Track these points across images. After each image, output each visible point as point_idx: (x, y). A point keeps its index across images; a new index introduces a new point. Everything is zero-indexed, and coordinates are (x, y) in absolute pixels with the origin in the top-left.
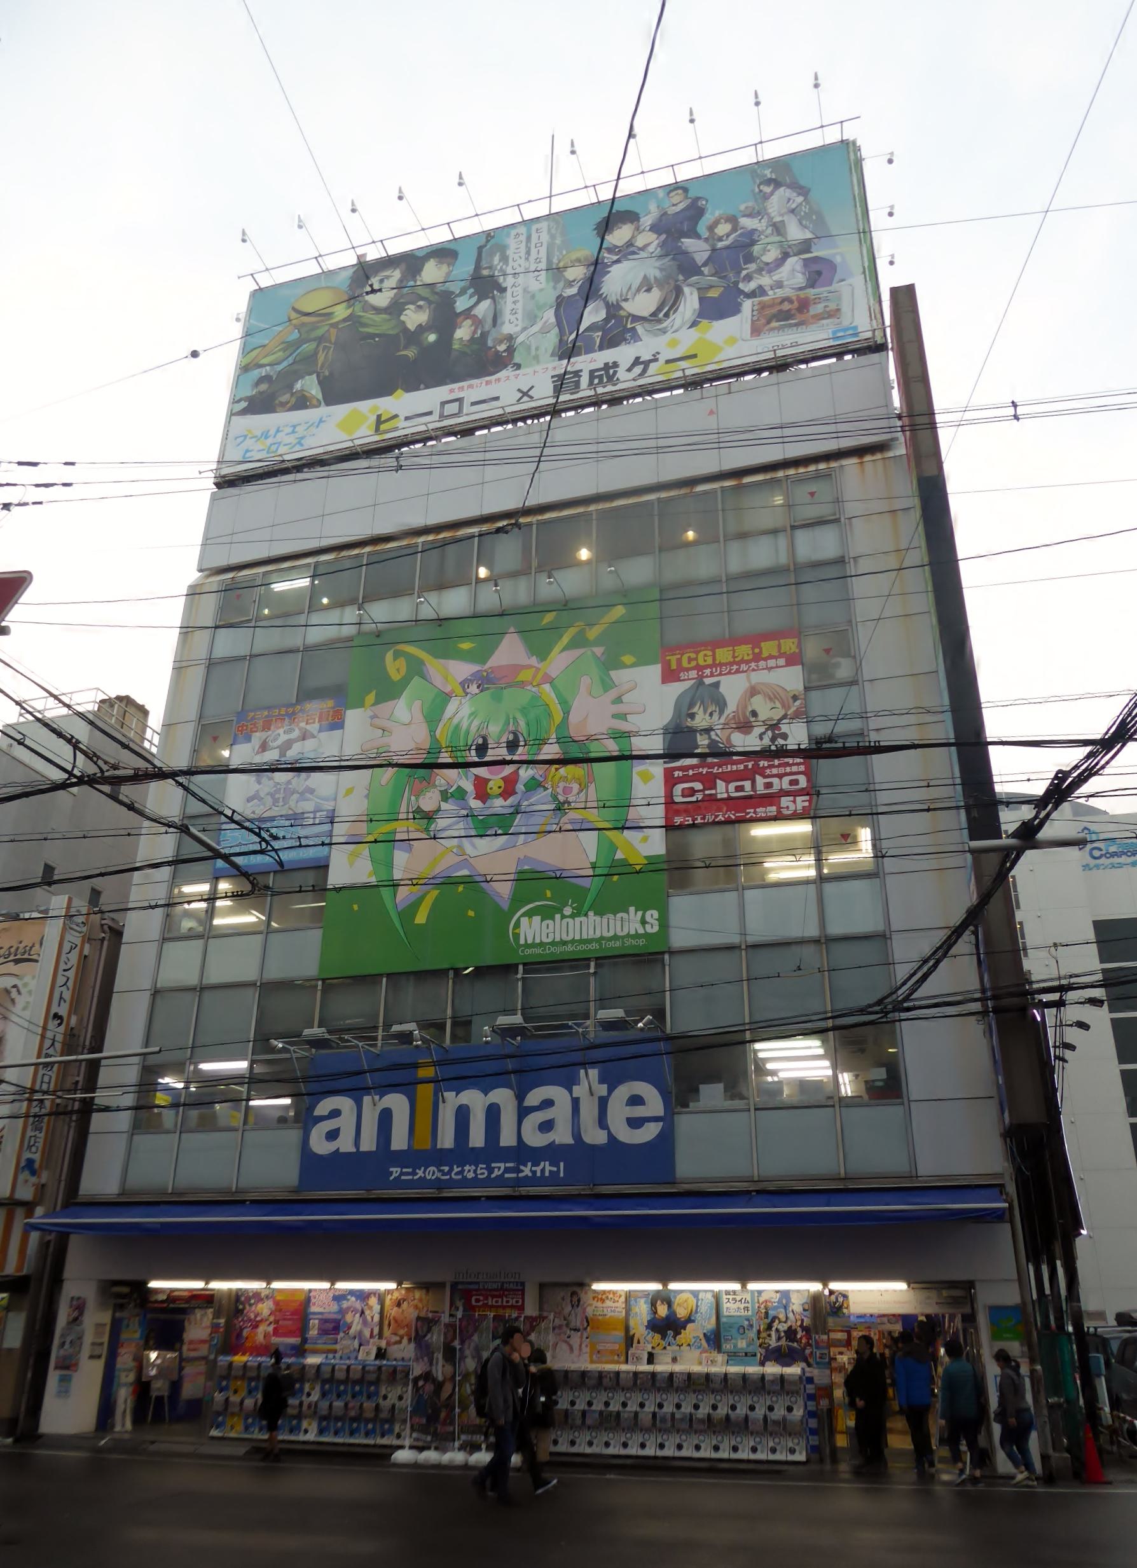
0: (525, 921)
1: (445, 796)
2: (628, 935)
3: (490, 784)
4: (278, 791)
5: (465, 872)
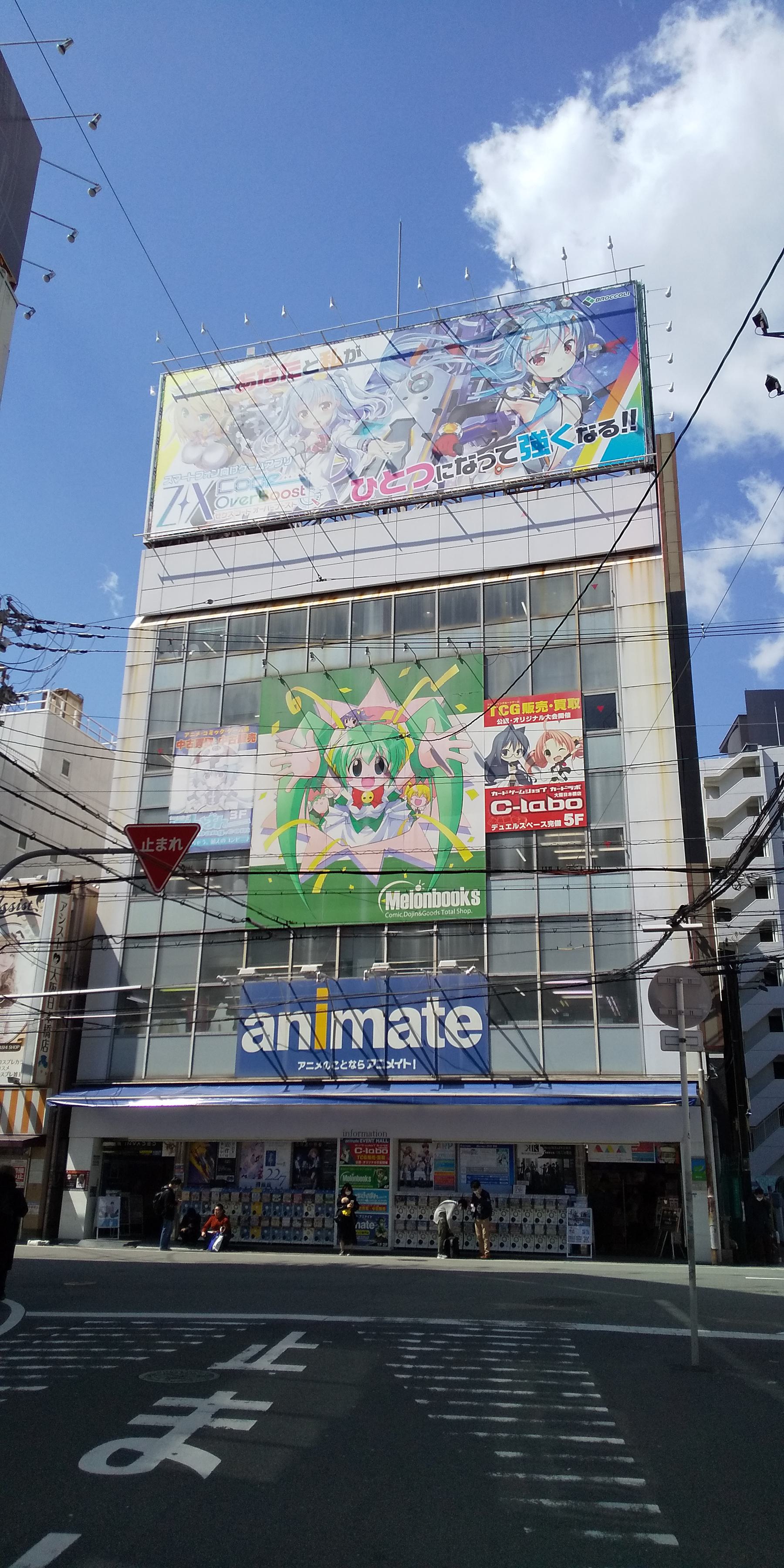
1: (332, 802)
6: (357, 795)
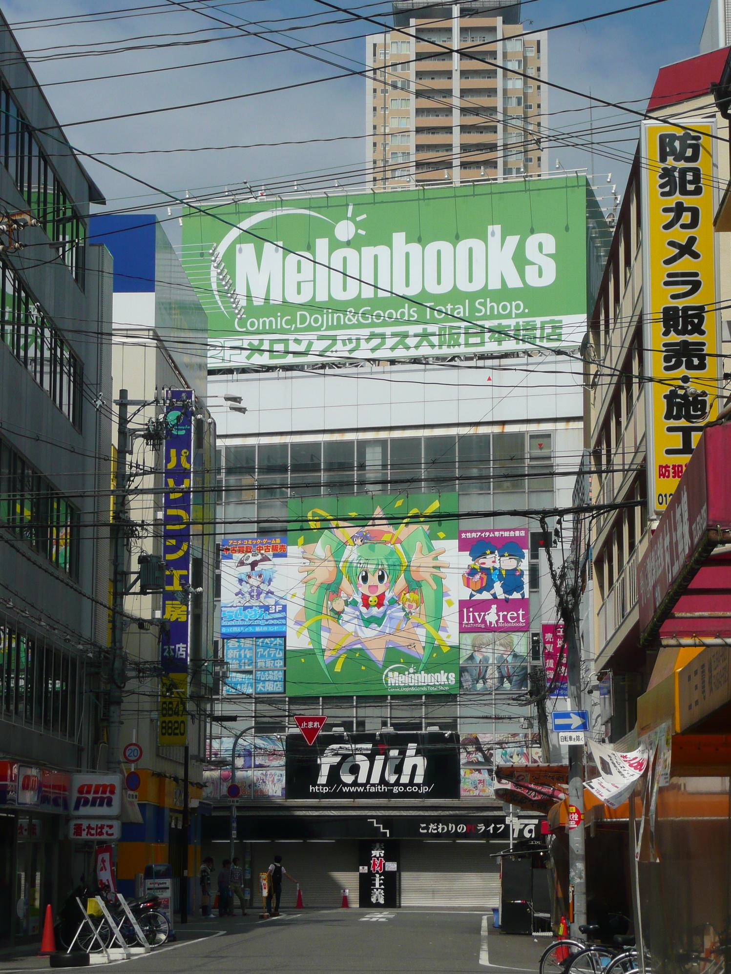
0: (390, 674)
1: (347, 603)
2: (485, 292)
3: (370, 599)
4: (253, 591)
5: (359, 646)
6: (365, 598)
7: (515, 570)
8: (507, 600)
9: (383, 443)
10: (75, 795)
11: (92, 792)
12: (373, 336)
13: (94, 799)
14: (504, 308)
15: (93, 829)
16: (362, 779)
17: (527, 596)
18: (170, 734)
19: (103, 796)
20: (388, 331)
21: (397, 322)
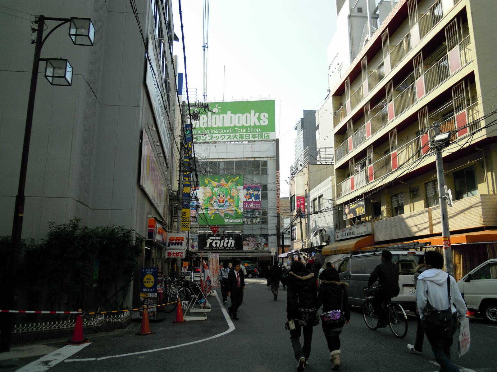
1: (215, 202)
2: (250, 126)
6: (219, 201)
7: (257, 194)
8: (255, 201)
9: (224, 162)
10: (168, 241)
11: (175, 240)
12: (222, 136)
13: (176, 243)
14: (255, 130)
15: (175, 254)
16: (218, 246)
17: (260, 200)
18: (184, 227)
19: (179, 242)
20: (226, 135)
21: (228, 133)
